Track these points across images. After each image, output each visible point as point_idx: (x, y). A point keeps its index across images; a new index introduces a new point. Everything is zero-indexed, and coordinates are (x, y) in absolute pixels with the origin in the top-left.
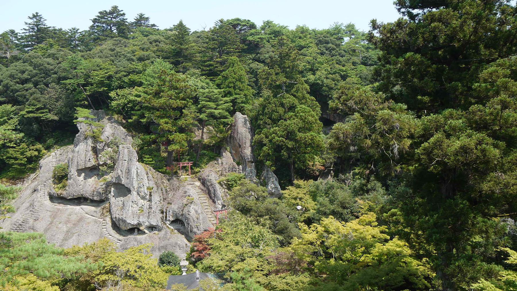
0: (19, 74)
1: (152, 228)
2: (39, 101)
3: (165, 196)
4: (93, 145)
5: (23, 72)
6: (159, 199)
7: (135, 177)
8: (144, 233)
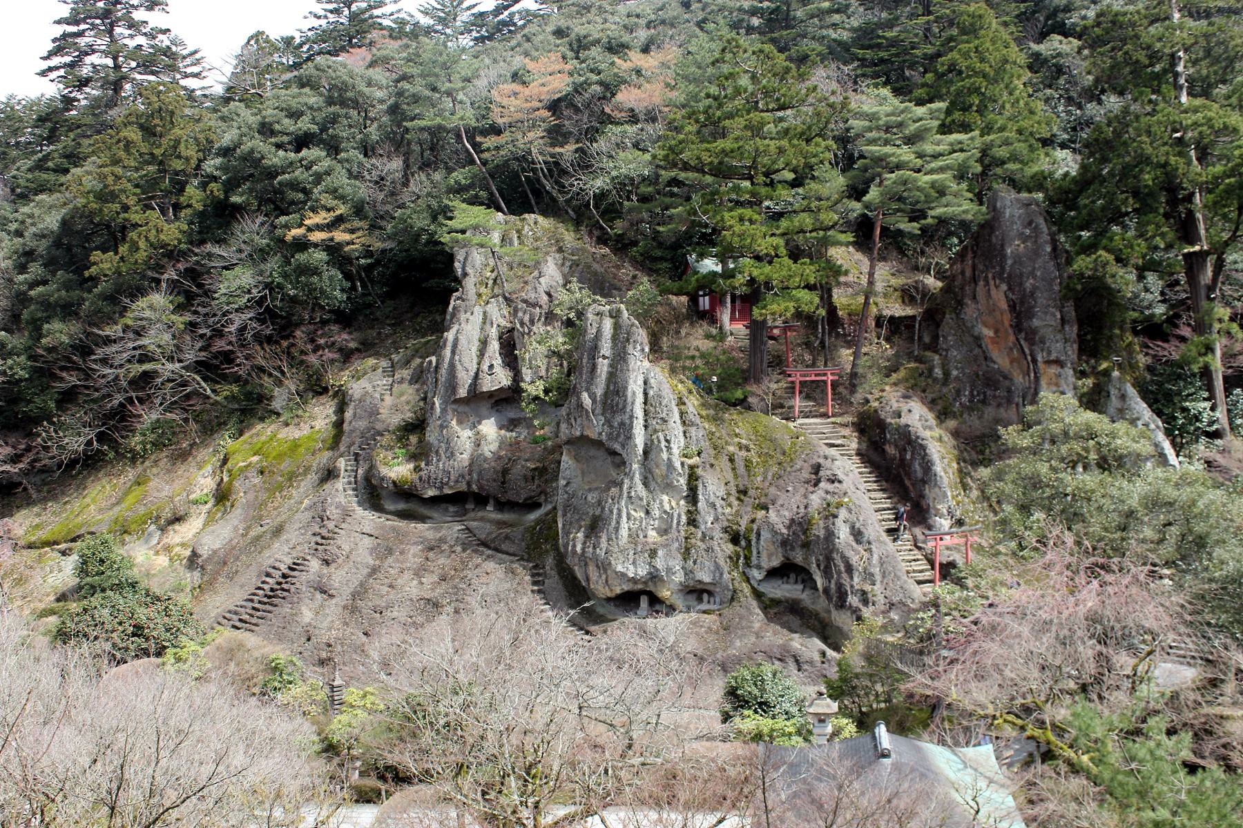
0: (286, 121)
1: (697, 592)
2: (342, 198)
3: (742, 483)
4: (503, 323)
5: (295, 115)
6: (722, 493)
7: (639, 412)
8: (671, 609)
